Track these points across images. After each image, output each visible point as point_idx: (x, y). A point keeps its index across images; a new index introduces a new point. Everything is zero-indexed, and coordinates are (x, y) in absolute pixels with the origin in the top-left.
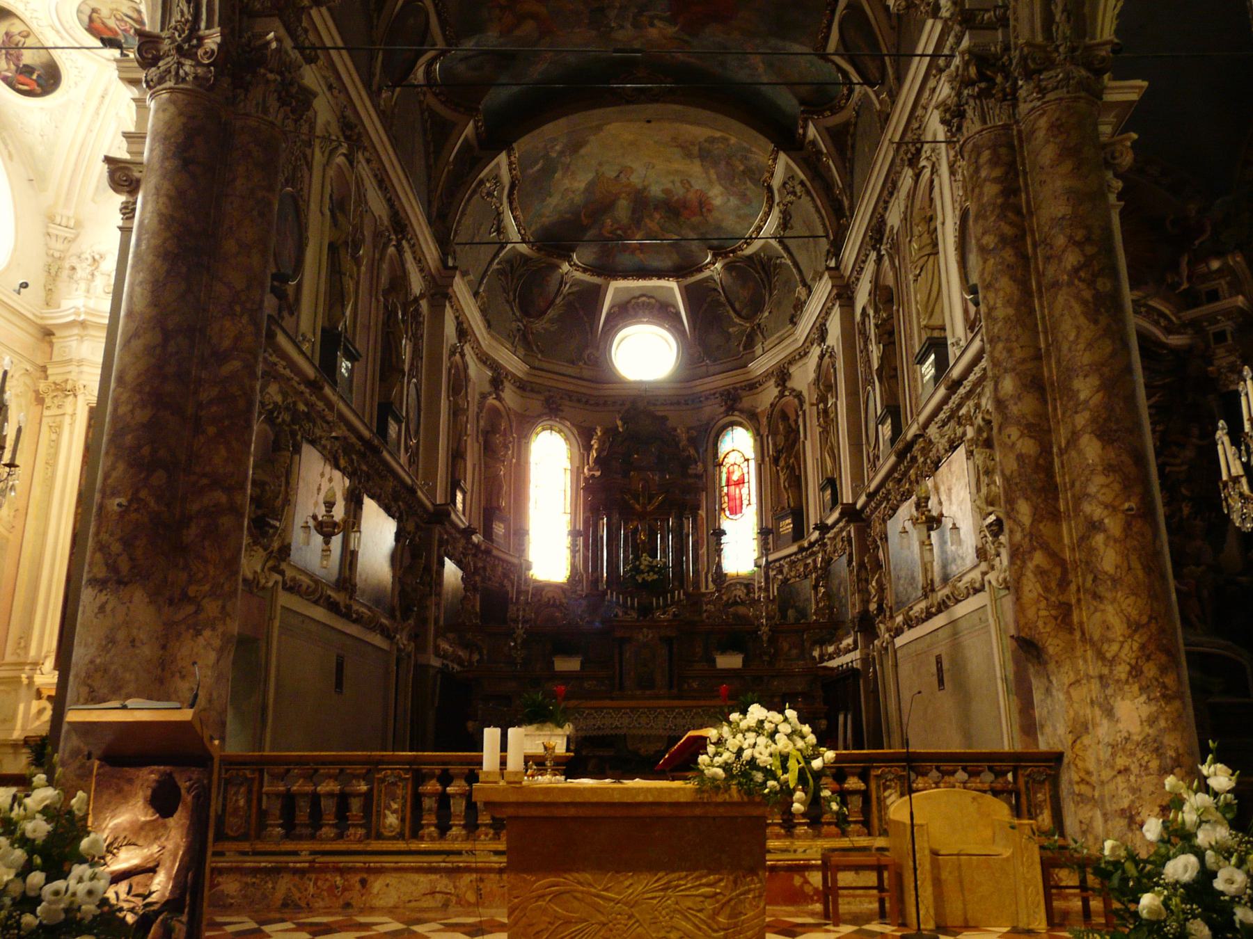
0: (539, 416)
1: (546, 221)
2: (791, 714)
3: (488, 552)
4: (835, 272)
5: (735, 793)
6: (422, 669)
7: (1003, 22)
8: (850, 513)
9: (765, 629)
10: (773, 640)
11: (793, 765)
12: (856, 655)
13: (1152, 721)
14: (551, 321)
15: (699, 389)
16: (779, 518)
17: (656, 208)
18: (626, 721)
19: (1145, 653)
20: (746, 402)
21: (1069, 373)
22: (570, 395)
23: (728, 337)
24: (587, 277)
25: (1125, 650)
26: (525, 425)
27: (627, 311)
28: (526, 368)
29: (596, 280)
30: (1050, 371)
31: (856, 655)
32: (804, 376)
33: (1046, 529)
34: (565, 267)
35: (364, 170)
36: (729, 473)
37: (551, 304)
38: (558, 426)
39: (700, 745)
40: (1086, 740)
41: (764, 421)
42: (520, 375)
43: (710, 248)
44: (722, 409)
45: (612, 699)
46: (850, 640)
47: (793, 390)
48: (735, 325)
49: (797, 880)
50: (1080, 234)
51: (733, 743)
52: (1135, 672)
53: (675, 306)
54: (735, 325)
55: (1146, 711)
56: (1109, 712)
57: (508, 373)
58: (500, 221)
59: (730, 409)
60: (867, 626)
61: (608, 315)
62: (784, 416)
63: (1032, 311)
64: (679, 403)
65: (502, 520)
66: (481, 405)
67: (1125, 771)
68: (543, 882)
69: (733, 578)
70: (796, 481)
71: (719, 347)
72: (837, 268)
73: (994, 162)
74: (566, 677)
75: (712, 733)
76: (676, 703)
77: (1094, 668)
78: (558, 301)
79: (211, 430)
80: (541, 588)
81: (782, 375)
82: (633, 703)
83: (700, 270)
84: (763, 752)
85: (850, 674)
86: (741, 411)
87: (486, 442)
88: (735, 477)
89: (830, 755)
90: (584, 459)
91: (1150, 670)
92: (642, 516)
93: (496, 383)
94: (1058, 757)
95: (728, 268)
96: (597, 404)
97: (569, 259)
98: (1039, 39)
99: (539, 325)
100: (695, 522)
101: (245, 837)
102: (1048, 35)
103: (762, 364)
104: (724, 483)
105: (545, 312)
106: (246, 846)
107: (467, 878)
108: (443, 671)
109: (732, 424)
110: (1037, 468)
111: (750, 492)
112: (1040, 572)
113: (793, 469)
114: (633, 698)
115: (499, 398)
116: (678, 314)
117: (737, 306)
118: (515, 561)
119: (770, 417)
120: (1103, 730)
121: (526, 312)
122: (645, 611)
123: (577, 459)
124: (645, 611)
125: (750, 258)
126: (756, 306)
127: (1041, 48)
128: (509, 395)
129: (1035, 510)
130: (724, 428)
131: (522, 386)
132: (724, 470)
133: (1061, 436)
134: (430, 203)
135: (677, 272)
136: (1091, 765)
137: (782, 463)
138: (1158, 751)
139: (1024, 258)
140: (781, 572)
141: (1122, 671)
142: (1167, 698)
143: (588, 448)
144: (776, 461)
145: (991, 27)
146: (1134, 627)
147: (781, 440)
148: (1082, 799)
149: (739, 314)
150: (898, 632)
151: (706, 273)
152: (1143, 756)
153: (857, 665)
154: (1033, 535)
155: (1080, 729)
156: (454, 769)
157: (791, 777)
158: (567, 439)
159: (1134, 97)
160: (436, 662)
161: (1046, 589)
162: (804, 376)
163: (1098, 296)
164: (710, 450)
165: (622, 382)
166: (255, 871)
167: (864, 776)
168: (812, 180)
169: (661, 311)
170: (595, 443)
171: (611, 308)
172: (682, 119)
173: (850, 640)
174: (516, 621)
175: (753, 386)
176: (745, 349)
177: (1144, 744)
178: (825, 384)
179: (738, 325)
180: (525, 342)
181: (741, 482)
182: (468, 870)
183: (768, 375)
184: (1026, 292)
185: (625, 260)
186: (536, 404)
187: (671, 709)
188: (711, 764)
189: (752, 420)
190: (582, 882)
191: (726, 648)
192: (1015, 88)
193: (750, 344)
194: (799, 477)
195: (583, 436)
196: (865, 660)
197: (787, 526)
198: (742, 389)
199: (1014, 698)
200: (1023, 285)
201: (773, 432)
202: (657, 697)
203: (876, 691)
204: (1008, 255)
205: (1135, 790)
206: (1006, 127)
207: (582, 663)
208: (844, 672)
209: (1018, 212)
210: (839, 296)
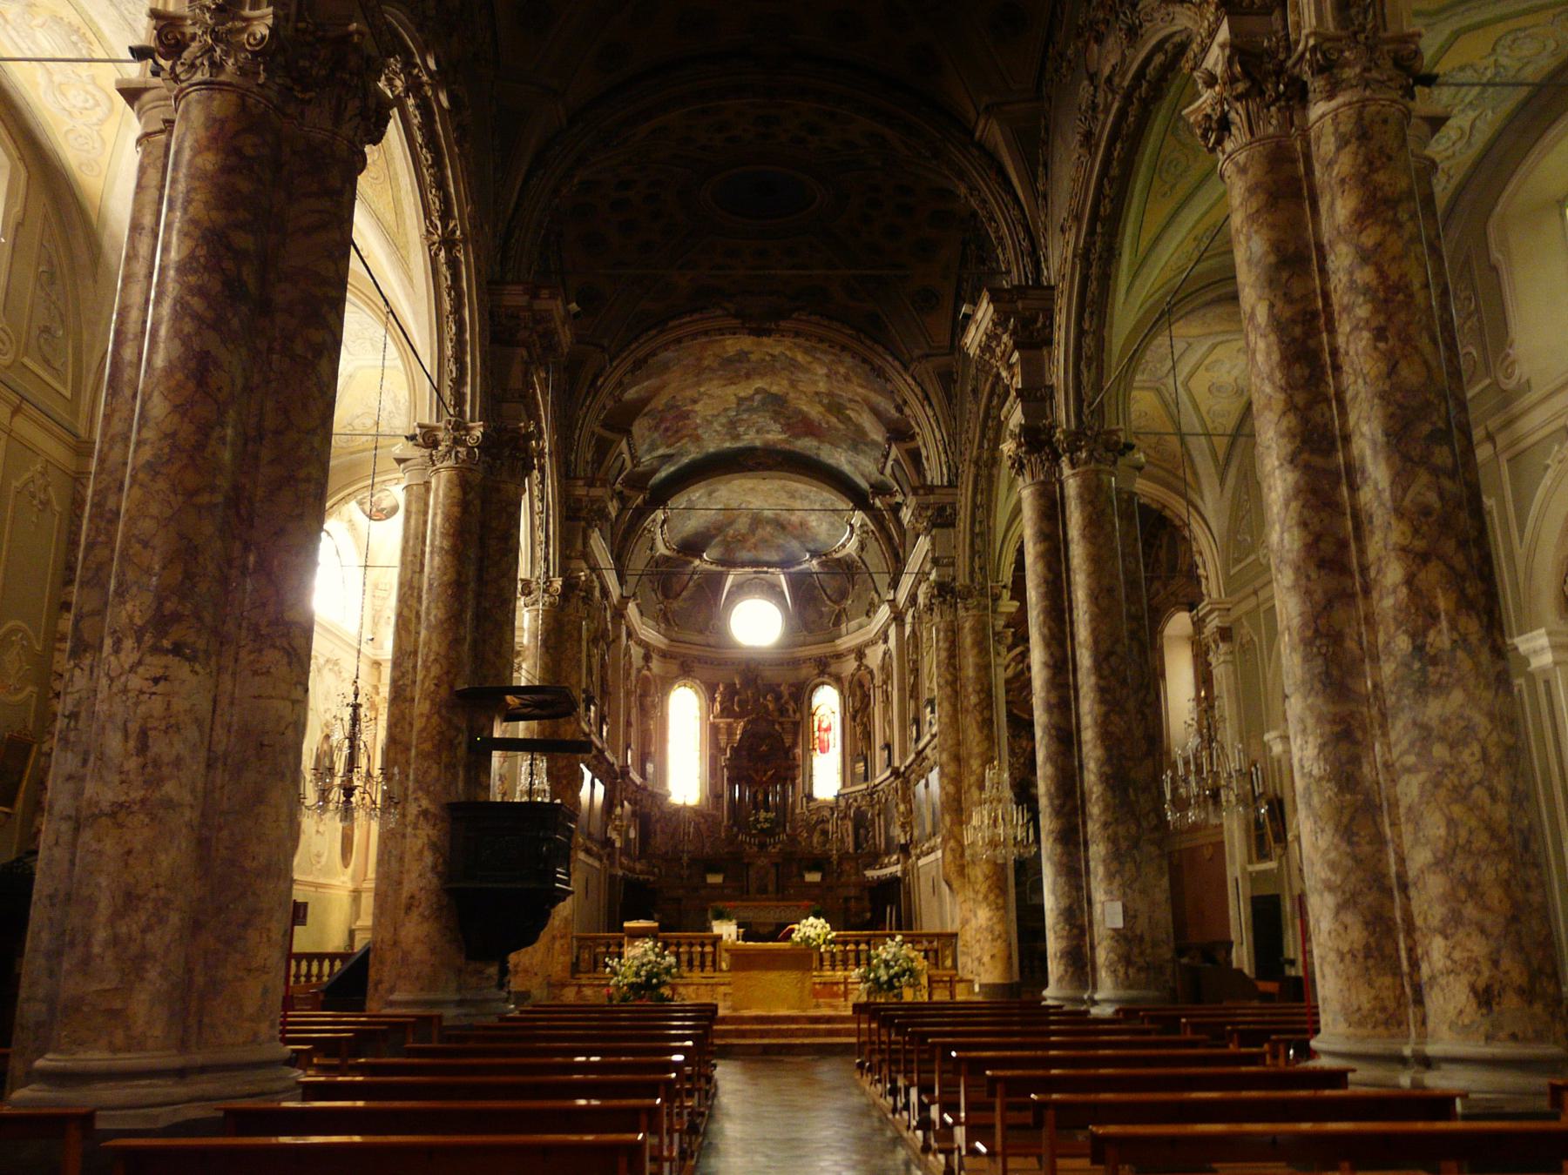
0: (677, 677)
1: (685, 534)
2: (822, 920)
3: (645, 789)
4: (892, 603)
5: (803, 945)
6: (612, 877)
7: (953, 564)
8: (896, 773)
9: (835, 857)
10: (839, 864)
11: (822, 938)
12: (899, 867)
13: (990, 919)
14: (685, 600)
15: (799, 654)
16: (854, 762)
17: (767, 523)
18: (751, 914)
19: (990, 889)
20: (833, 669)
21: (970, 755)
22: (699, 659)
23: (821, 615)
24: (713, 567)
25: (983, 888)
26: (666, 684)
27: (740, 590)
28: (666, 641)
29: (720, 569)
30: (963, 752)
31: (899, 867)
32: (874, 657)
33: (956, 829)
34: (697, 562)
35: (594, 577)
36: (820, 722)
37: (685, 587)
38: (689, 683)
39: (792, 930)
40: (967, 927)
41: (846, 685)
42: (663, 647)
43: (808, 551)
44: (816, 672)
45: (743, 900)
46: (895, 857)
47: (867, 667)
48: (826, 605)
49: (835, 988)
50: (978, 687)
51: (803, 930)
52: (986, 897)
53: (780, 586)
54: (826, 605)
55: (991, 914)
56: (975, 915)
57: (655, 648)
58: (653, 544)
59: (822, 673)
60: (905, 850)
61: (729, 592)
62: (861, 685)
63: (957, 720)
64: (782, 664)
65: (652, 762)
66: (637, 676)
67: (979, 941)
68: (742, 974)
69: (822, 802)
70: (868, 736)
71: (814, 622)
72: (894, 600)
73: (946, 639)
74: (714, 886)
75: (796, 926)
76: (781, 903)
77: (972, 895)
78: (691, 584)
79: (564, 782)
80: (679, 810)
81: (860, 654)
82: (756, 904)
83: (800, 564)
84: (812, 933)
85: (894, 881)
86: (830, 675)
87: (641, 705)
88: (824, 725)
89: (834, 934)
90: (710, 709)
91: (992, 897)
92: (761, 783)
93: (647, 658)
94: (955, 935)
95: (821, 564)
96: (719, 664)
97: (701, 557)
98: (968, 581)
99: (676, 605)
100: (793, 788)
101: (589, 972)
102: (972, 580)
103: (846, 642)
104: (816, 729)
105: (679, 595)
106: (590, 975)
107: (691, 988)
108: (624, 877)
109: (823, 683)
110: (954, 800)
111: (835, 738)
112: (952, 850)
113: (865, 726)
114: (754, 900)
115: (649, 669)
116: (783, 592)
117: (828, 591)
118: (660, 791)
119: (851, 683)
120: (973, 923)
121: (666, 596)
122: (762, 846)
123: (704, 709)
124: (762, 846)
125: (839, 560)
126: (843, 595)
127: (968, 587)
128: (656, 665)
129: (952, 820)
130: (817, 686)
131: (664, 655)
132: (816, 718)
133: (966, 786)
134: (612, 544)
135: (783, 564)
136: (968, 939)
137: (858, 720)
138: (992, 932)
139: (956, 693)
140: (856, 800)
141: (980, 897)
142: (998, 909)
143: (713, 700)
144: (854, 718)
145: (947, 565)
146: (987, 878)
147: (858, 705)
148: (964, 953)
149: (829, 598)
150: (918, 858)
151: (805, 566)
152: (985, 934)
153: (899, 874)
154: (950, 832)
155: (965, 922)
156: (682, 941)
157: (821, 941)
158: (697, 692)
159: (1013, 610)
160: (620, 873)
161: (954, 857)
162: (874, 657)
163: (984, 720)
164: (806, 703)
165: (736, 646)
166: (599, 985)
167: (868, 943)
168: (880, 532)
169: (773, 591)
170: (718, 697)
171: (732, 586)
172: (790, 480)
173: (895, 857)
174: (683, 852)
175: (839, 656)
176: (834, 625)
177: (986, 929)
178: (885, 667)
179: (828, 607)
180: (666, 619)
181: (828, 729)
182: (692, 984)
183: (850, 651)
184: (955, 711)
185: (744, 555)
186: (674, 667)
187: (777, 907)
188: (796, 937)
189: (838, 681)
190: (755, 974)
191: (810, 869)
192: (956, 603)
193: (837, 623)
194: (869, 733)
195: (710, 689)
196: (905, 872)
197: (860, 767)
198: (832, 657)
199: (1062, 880)
200: (954, 706)
201: (853, 695)
202: (769, 900)
203: (909, 893)
204: (948, 690)
205: (982, 949)
206: (952, 622)
207: (724, 878)
208: (887, 879)
209: (955, 668)
210: (895, 619)
